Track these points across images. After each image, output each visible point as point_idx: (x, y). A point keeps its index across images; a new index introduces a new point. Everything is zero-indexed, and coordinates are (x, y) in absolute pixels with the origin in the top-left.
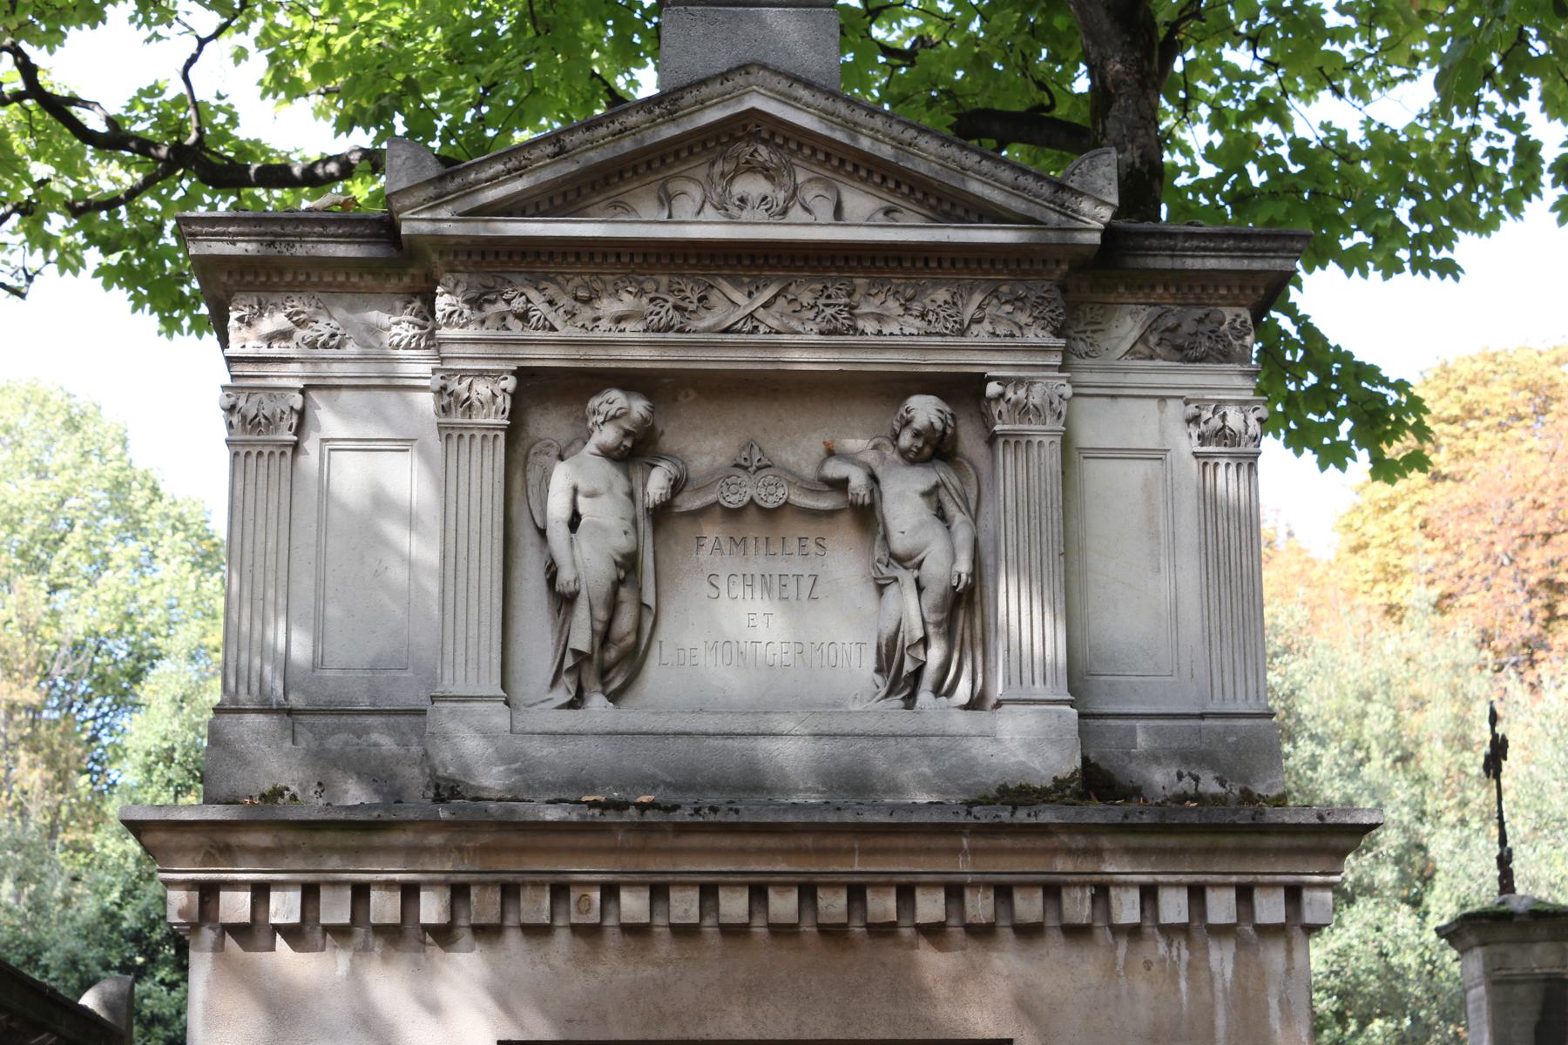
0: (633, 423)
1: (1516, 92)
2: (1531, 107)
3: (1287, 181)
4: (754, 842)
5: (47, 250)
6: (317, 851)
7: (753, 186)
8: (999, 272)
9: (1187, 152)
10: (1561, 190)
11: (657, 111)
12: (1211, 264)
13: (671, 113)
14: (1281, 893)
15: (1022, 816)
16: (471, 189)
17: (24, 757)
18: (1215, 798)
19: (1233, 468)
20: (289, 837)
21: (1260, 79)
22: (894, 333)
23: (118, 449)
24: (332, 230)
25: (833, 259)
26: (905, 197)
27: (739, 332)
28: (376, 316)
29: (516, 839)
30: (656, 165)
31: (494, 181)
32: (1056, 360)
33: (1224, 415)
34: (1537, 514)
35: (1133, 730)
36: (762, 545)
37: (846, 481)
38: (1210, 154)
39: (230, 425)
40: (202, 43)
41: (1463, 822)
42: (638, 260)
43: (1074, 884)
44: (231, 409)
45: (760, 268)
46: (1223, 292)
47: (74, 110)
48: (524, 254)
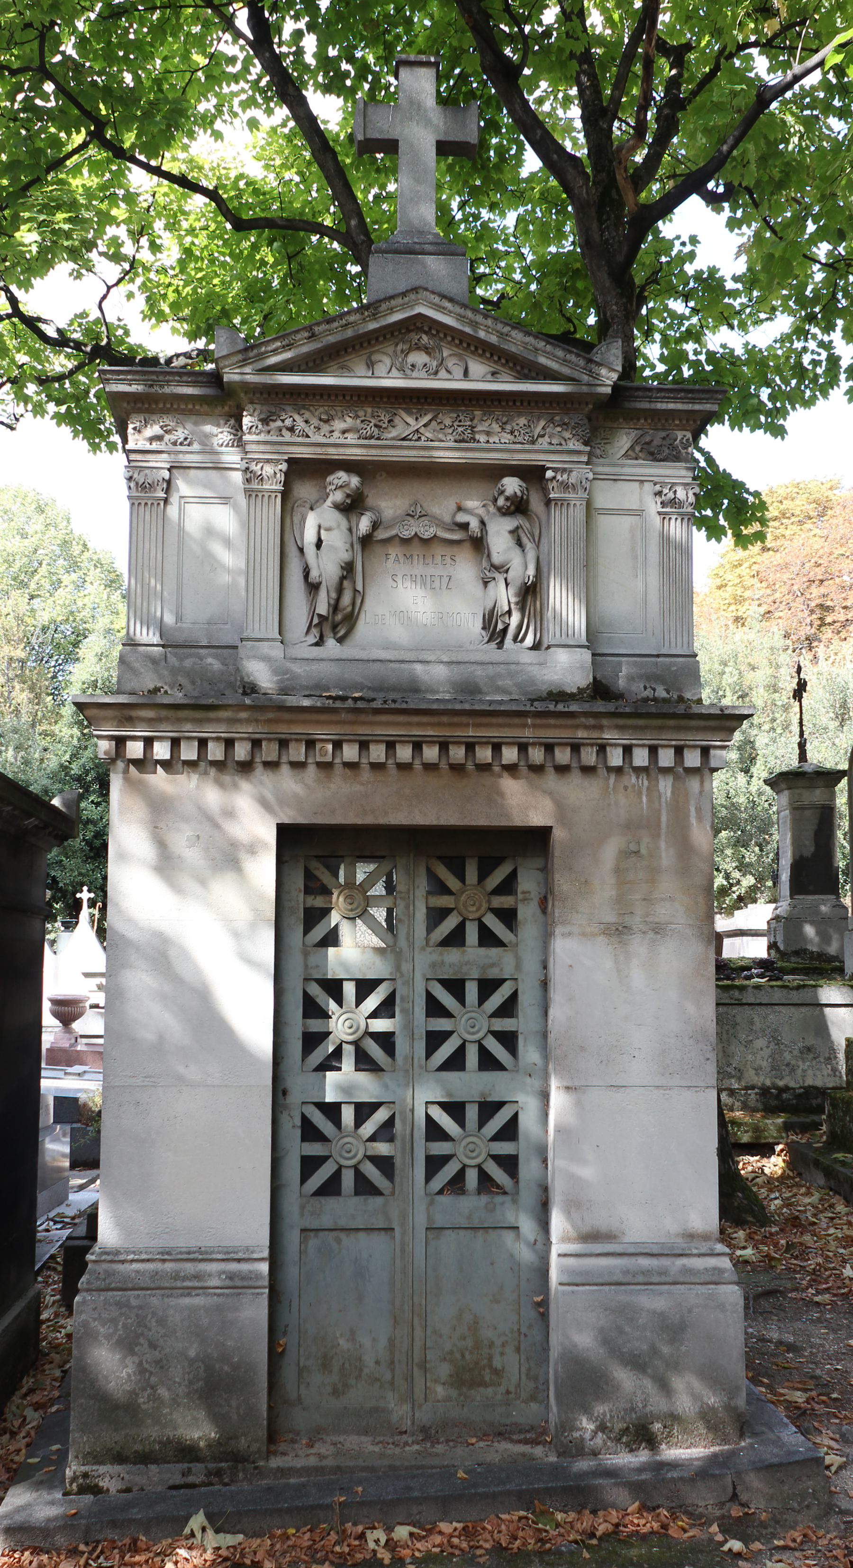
0: (351, 490)
1: (829, 328)
2: (837, 337)
3: (703, 375)
4: (416, 719)
5: (26, 404)
6: (179, 720)
7: (418, 358)
8: (554, 409)
9: (646, 359)
10: (851, 383)
11: (366, 313)
12: (671, 406)
13: (374, 315)
14: (699, 751)
15: (560, 707)
16: (262, 356)
17: (18, 686)
18: (664, 700)
19: (679, 520)
20: (164, 713)
21: (688, 319)
22: (496, 442)
23: (65, 523)
24: (185, 378)
25: (463, 399)
26: (503, 365)
27: (410, 440)
28: (208, 428)
29: (287, 716)
30: (365, 345)
31: (275, 352)
32: (585, 459)
33: (675, 492)
34: (817, 570)
35: (620, 664)
36: (421, 559)
37: (468, 524)
38: (662, 359)
39: (130, 488)
40: (109, 288)
41: (773, 729)
42: (355, 398)
43: (588, 745)
44: (130, 479)
45: (422, 404)
46: (677, 422)
47: (40, 324)
48: (292, 394)
